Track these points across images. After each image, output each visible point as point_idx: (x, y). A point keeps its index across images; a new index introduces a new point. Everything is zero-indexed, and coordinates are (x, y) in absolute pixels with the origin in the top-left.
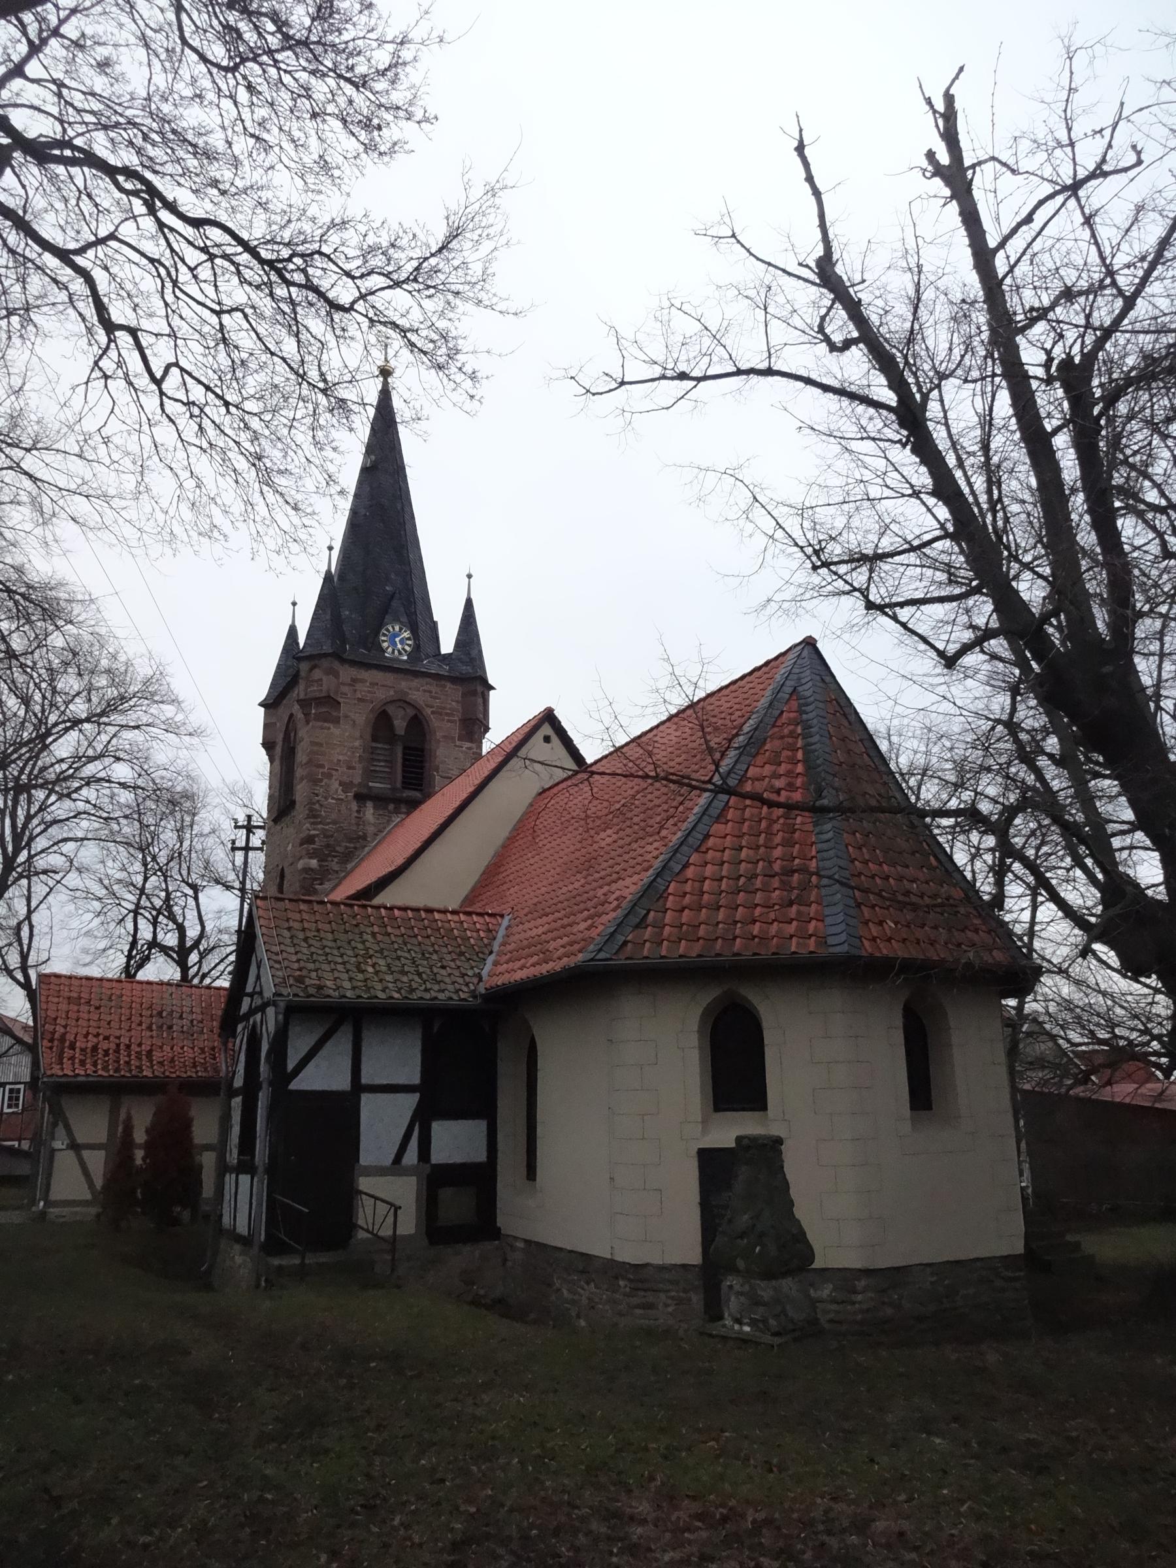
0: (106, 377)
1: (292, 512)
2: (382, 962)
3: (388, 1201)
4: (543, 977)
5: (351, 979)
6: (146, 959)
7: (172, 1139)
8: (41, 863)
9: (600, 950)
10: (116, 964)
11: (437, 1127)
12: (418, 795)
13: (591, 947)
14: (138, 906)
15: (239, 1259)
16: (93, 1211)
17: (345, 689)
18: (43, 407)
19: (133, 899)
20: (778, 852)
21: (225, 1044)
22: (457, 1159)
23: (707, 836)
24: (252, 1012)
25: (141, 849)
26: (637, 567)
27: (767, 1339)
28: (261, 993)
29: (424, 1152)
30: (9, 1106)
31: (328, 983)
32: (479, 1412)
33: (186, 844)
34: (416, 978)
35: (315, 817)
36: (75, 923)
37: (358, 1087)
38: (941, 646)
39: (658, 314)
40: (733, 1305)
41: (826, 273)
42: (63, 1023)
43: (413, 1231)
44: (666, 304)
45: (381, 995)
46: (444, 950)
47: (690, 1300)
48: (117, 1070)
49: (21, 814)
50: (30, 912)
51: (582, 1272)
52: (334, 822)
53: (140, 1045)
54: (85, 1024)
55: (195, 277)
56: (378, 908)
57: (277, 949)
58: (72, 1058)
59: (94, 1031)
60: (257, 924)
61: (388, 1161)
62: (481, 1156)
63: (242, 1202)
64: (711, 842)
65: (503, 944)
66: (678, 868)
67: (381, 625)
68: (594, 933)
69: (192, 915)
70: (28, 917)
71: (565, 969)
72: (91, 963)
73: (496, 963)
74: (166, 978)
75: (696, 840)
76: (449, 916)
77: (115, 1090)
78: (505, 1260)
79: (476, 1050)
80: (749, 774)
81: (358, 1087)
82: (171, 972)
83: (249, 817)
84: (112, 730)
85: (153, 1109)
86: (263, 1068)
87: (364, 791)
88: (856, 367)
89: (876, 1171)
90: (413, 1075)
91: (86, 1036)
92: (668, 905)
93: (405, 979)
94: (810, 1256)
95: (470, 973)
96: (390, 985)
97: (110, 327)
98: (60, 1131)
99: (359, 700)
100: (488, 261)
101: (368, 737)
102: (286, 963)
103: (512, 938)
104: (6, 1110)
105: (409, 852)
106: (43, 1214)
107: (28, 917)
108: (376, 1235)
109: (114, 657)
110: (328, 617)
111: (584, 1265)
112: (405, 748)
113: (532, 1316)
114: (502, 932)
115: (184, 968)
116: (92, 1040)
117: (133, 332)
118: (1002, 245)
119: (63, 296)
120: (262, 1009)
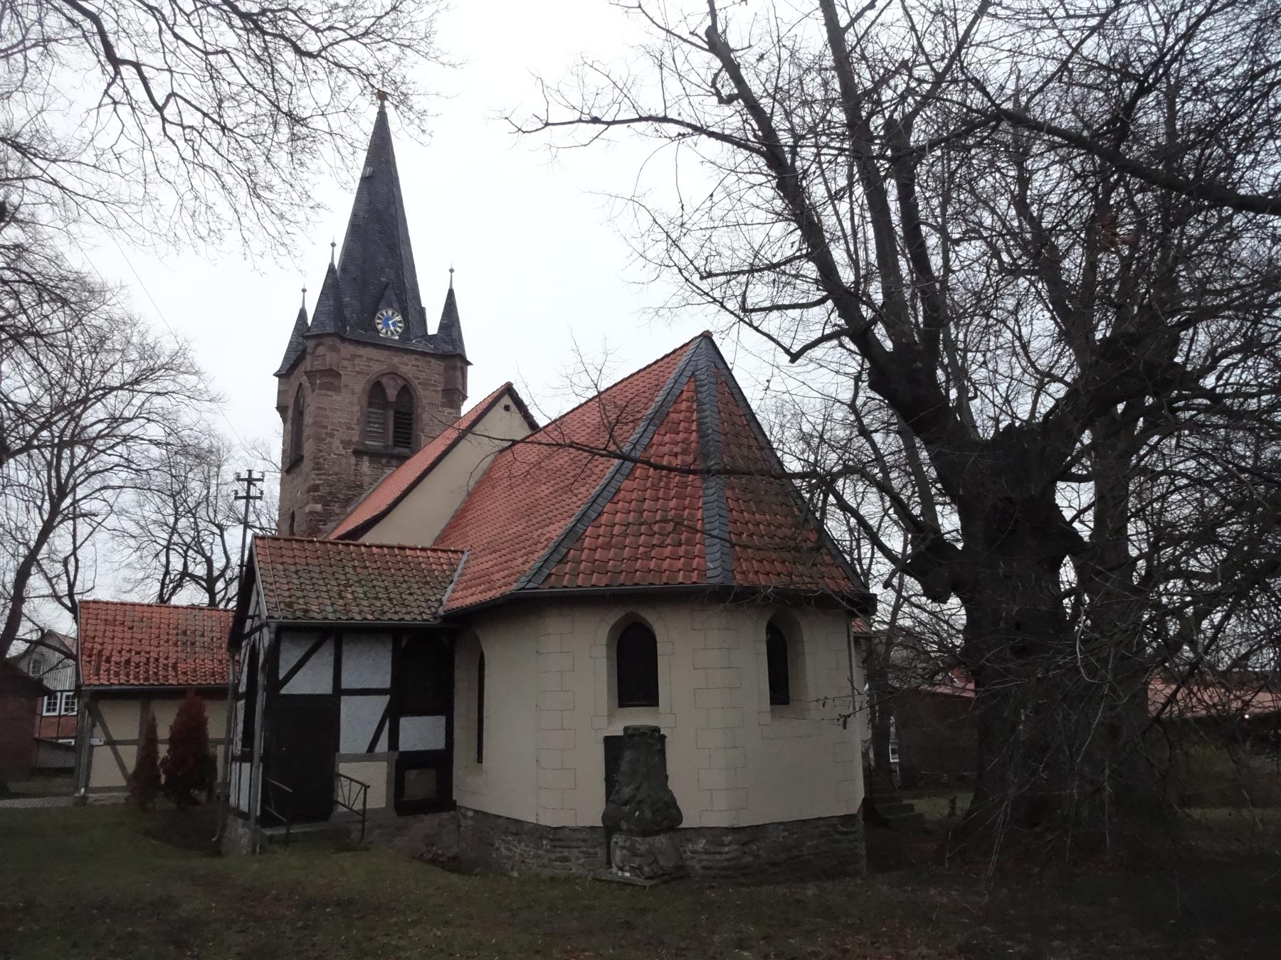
0: (115, 103)
1: (277, 221)
2: (360, 590)
3: (363, 782)
4: (487, 602)
5: (332, 604)
6: (179, 585)
7: (190, 734)
8: (85, 506)
9: (529, 581)
10: (152, 591)
11: (405, 722)
12: (406, 451)
13: (523, 579)
14: (169, 541)
15: (241, 831)
16: (127, 794)
17: (346, 363)
18: (62, 127)
19: (166, 536)
20: (673, 503)
21: (233, 657)
22: (420, 747)
23: (618, 490)
24: (253, 631)
25: (173, 496)
26: (585, 269)
27: (641, 881)
28: (259, 616)
30: (48, 710)
31: (314, 608)
32: (402, 943)
33: (213, 489)
34: (388, 603)
35: (318, 469)
36: (117, 557)
38: (787, 345)
39: (574, 69)
40: (618, 855)
41: (716, 43)
42: (100, 641)
43: (383, 805)
44: (581, 62)
45: (358, 617)
46: (413, 580)
47: (596, 854)
48: (147, 679)
49: (65, 468)
50: (75, 549)
51: (516, 834)
52: (336, 474)
53: (167, 658)
54: (120, 641)
55: (189, 22)
56: (358, 546)
57: (271, 580)
58: (108, 670)
59: (127, 648)
60: (256, 560)
61: (364, 750)
62: (440, 744)
63: (243, 785)
64: (621, 495)
65: (461, 575)
66: (594, 515)
67: (376, 310)
68: (526, 567)
69: (218, 550)
70: (74, 553)
71: (503, 596)
72: (131, 590)
73: (454, 591)
74: (196, 602)
75: (610, 493)
76: (419, 553)
77: (145, 696)
78: (459, 826)
79: (435, 660)
80: (654, 441)
82: (202, 598)
83: (250, 472)
84: (142, 397)
85: (177, 710)
86: (261, 678)
87: (360, 448)
88: (732, 118)
89: (745, 750)
90: (386, 682)
91: (120, 652)
92: (585, 545)
93: (378, 604)
94: (679, 818)
95: (433, 599)
96: (366, 609)
97: (116, 62)
98: (98, 729)
99: (358, 373)
100: (431, 21)
101: (365, 403)
102: (279, 592)
103: (469, 571)
104: (45, 714)
105: (390, 500)
106: (84, 798)
107: (74, 553)
108: (351, 809)
109: (142, 335)
110: (331, 303)
111: (516, 828)
112: (396, 412)
113: (478, 870)
114: (461, 566)
115: (212, 594)
116: (126, 656)
117: (137, 66)
118: (851, 24)
119: (79, 33)
120: (259, 628)
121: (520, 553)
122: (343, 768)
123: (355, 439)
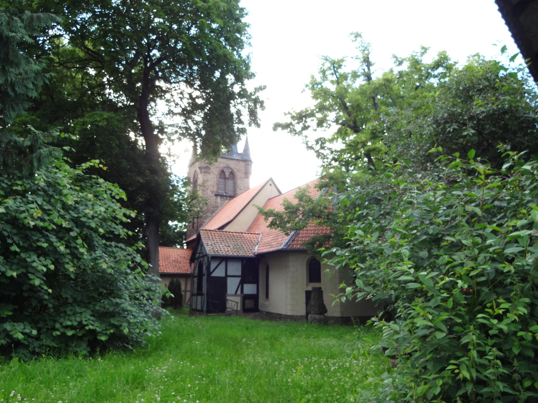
37: (227, 276)
61: (234, 293)
81: (227, 276)
87: (217, 193)
90: (239, 273)
121: (279, 237)
122: (228, 298)
123: (215, 190)
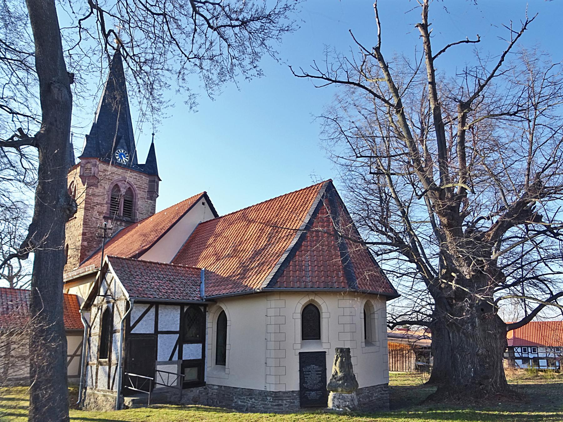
29: (180, 356)
47: (294, 402)
108: (167, 386)
112: (125, 200)
122: (159, 367)
